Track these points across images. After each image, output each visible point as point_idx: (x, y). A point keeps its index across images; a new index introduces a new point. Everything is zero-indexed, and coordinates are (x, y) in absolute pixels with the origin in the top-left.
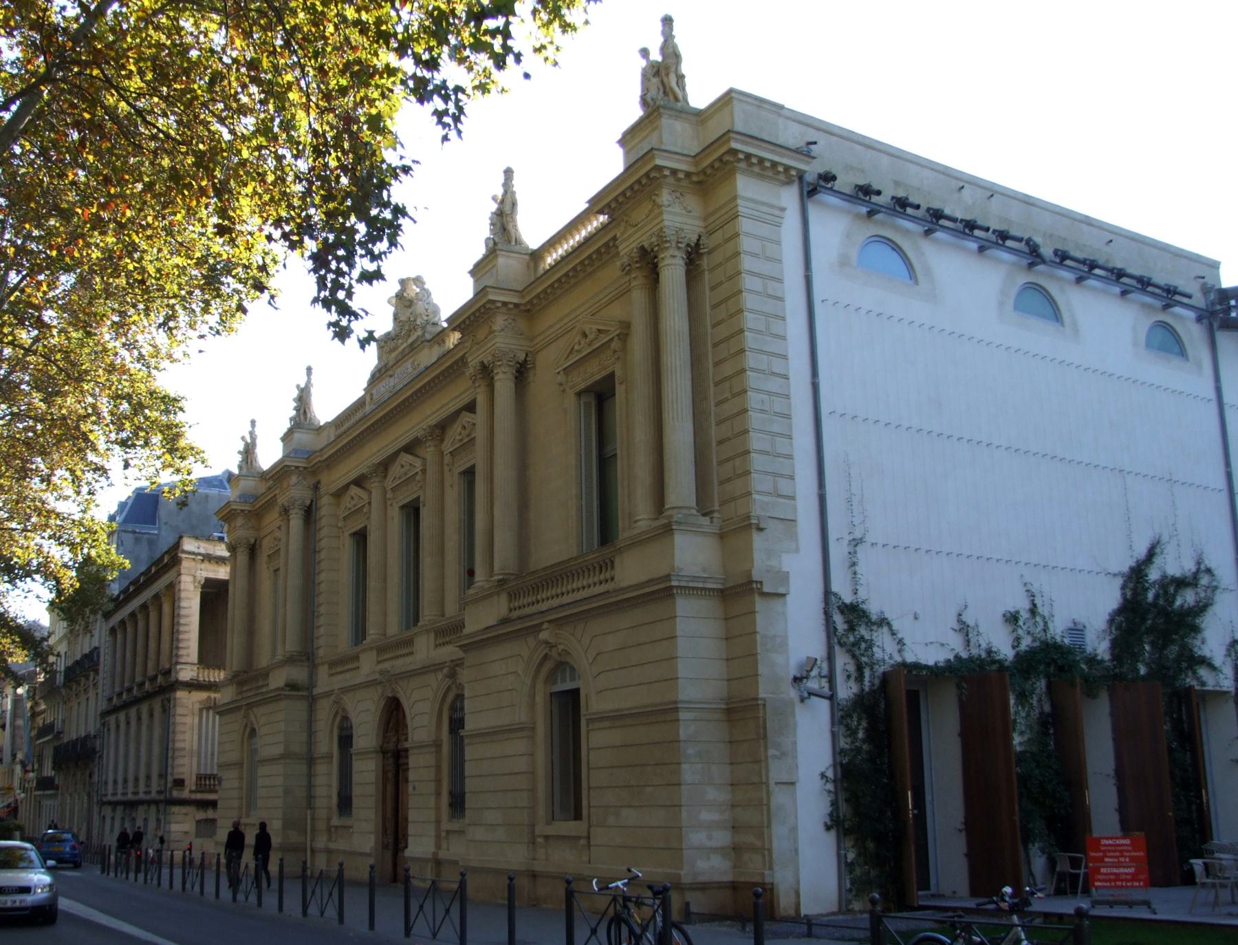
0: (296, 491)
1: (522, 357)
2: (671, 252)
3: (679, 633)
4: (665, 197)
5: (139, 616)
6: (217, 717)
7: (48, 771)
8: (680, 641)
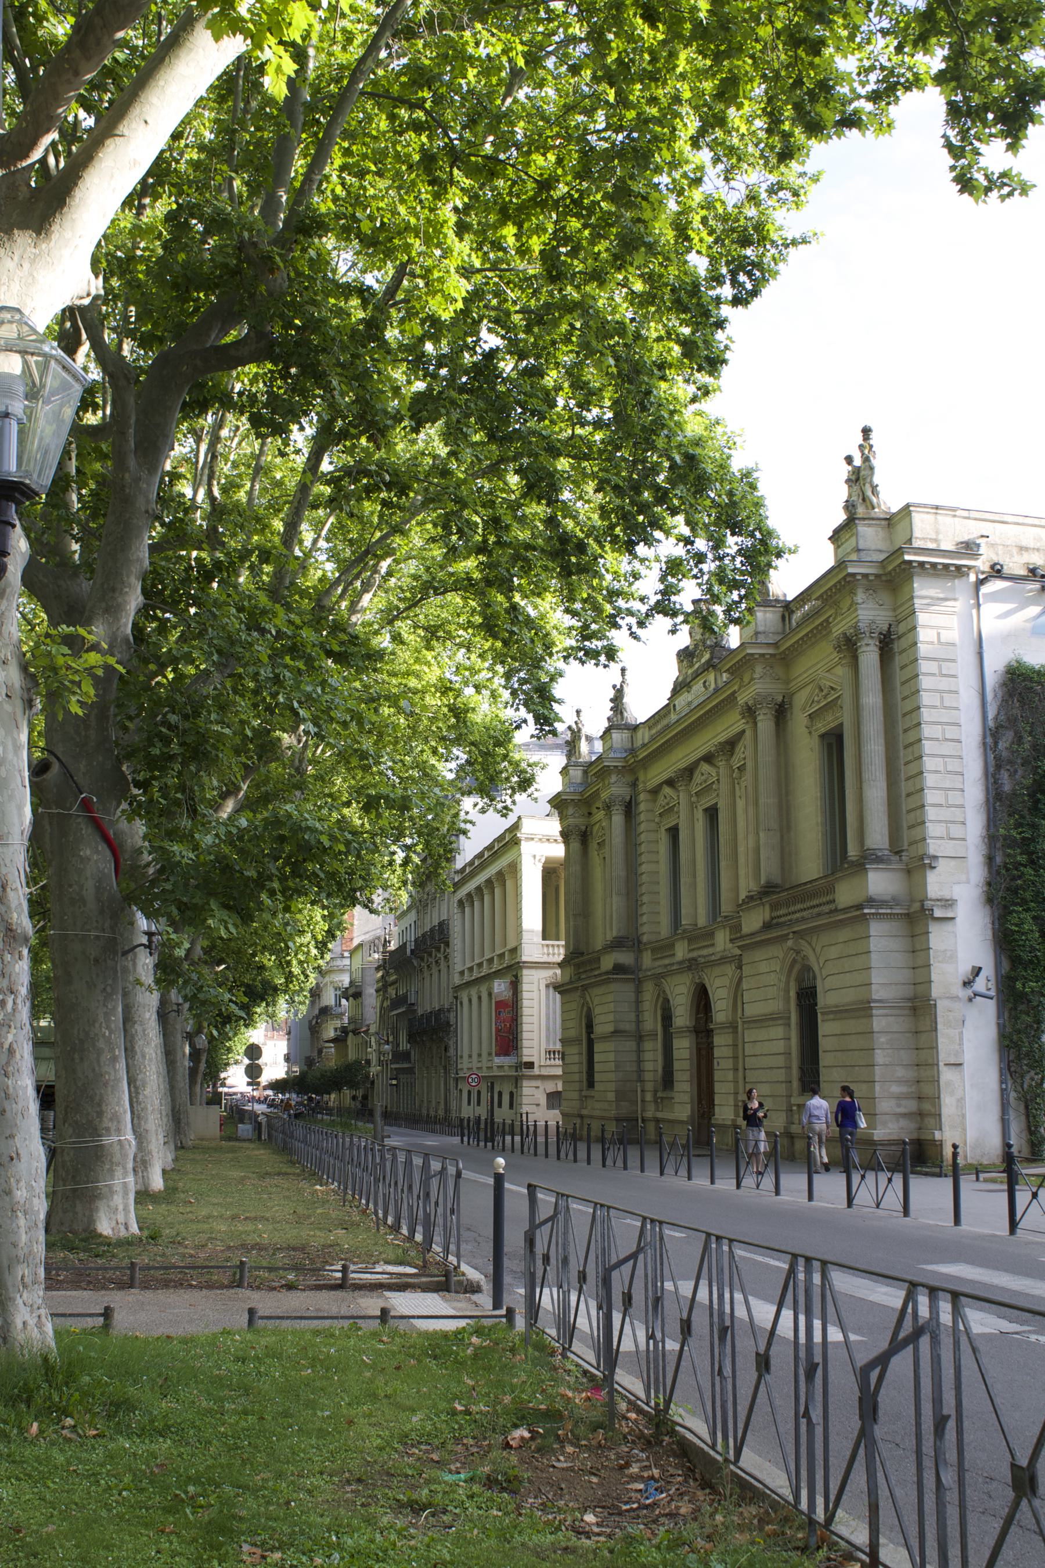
0: (616, 788)
1: (780, 699)
2: (866, 641)
3: (872, 948)
4: (860, 596)
5: (485, 891)
6: (558, 996)
7: (404, 1045)
8: (873, 956)
